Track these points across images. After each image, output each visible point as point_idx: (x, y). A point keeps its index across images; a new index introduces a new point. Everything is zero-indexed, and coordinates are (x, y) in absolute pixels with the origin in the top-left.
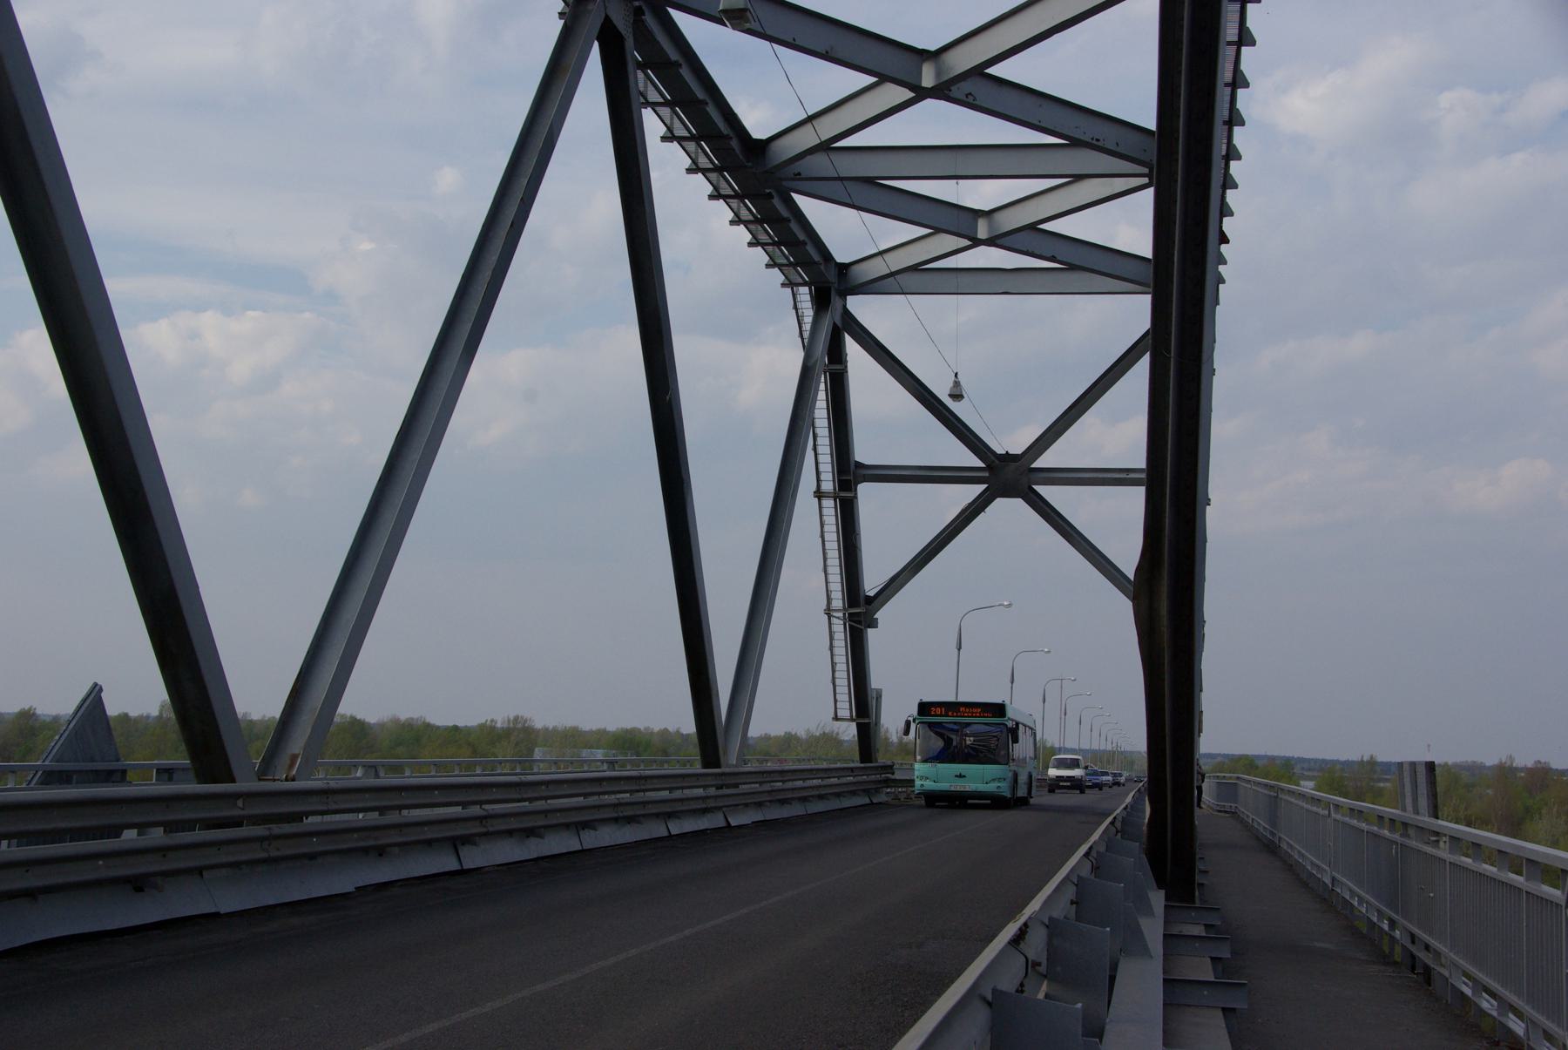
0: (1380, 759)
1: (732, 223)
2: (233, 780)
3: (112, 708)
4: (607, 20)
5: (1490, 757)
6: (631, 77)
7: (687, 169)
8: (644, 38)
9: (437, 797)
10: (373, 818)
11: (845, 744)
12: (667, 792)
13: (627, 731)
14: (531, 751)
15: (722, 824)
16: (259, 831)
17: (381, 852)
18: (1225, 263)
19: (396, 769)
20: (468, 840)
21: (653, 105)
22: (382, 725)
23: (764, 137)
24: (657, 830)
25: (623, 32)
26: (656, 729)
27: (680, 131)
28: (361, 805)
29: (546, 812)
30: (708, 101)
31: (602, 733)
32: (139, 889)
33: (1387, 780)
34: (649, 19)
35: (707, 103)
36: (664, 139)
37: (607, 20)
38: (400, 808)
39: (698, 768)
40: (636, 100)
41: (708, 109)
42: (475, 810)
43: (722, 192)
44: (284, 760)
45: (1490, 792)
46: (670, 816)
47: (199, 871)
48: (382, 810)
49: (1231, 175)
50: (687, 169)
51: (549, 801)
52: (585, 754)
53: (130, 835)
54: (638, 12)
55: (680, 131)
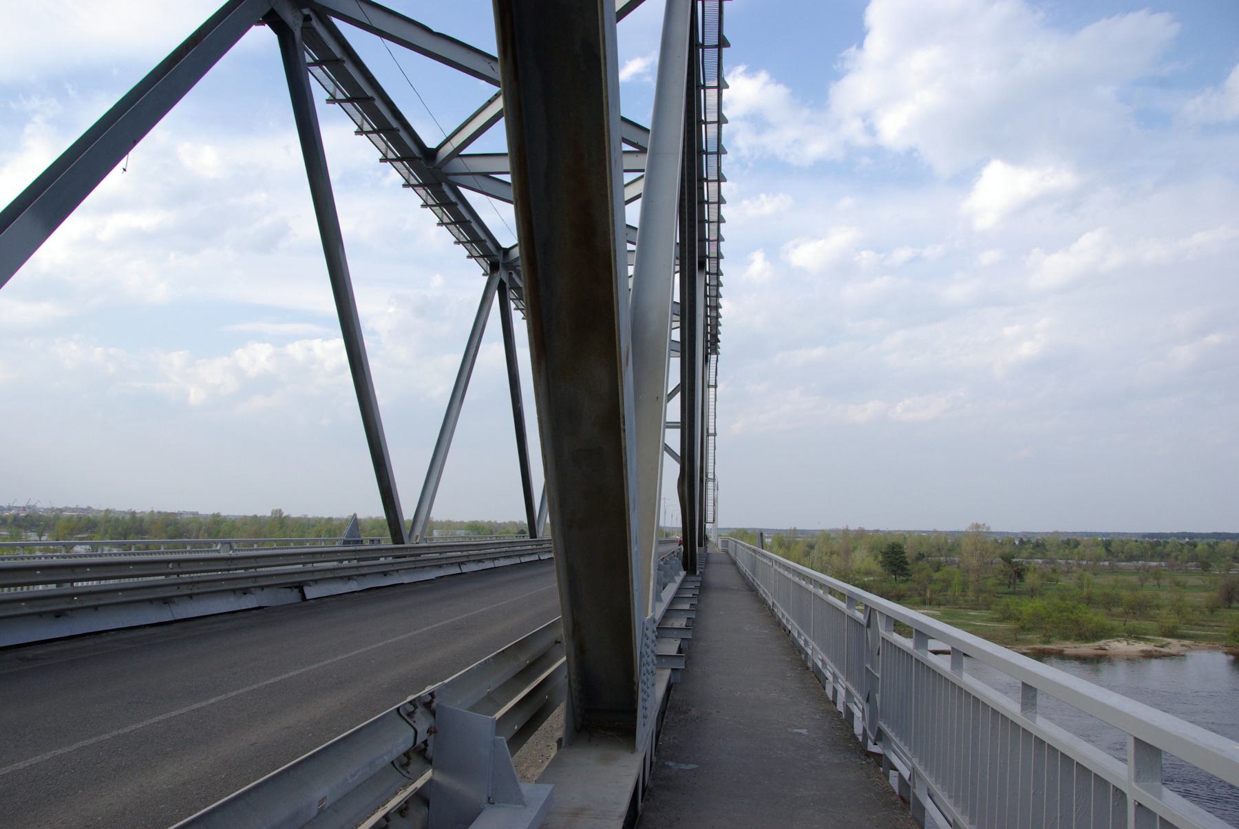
0: (798, 528)
1: (468, 257)
2: (404, 543)
3: (358, 517)
4: (501, 279)
5: (841, 526)
6: (508, 293)
7: (327, 100)
8: (319, 46)
9: (456, 549)
10: (437, 556)
11: (334, 522)
12: (460, 553)
13: (473, 522)
14: (431, 534)
15: (537, 558)
16: (413, 559)
17: (440, 566)
18: (719, 342)
19: (301, 543)
20: (463, 563)
21: (512, 299)
22: (365, 520)
23: (435, 147)
24: (516, 561)
25: (505, 281)
26: (486, 521)
27: (446, 220)
28: (218, 568)
29: (485, 554)
30: (345, 59)
31: (462, 523)
32: (385, 575)
33: (800, 538)
34: (315, 23)
35: (399, 130)
36: (328, 101)
37: (501, 279)
38: (446, 552)
39: (390, 545)
40: (508, 299)
41: (400, 134)
42: (465, 553)
43: (461, 240)
44: (414, 537)
45: (841, 541)
46: (521, 556)
47: (96, 608)
48: (440, 553)
49: (722, 216)
50: (327, 100)
51: (258, 570)
52: (458, 532)
53: (382, 560)
54: (307, 19)
55: (446, 220)
